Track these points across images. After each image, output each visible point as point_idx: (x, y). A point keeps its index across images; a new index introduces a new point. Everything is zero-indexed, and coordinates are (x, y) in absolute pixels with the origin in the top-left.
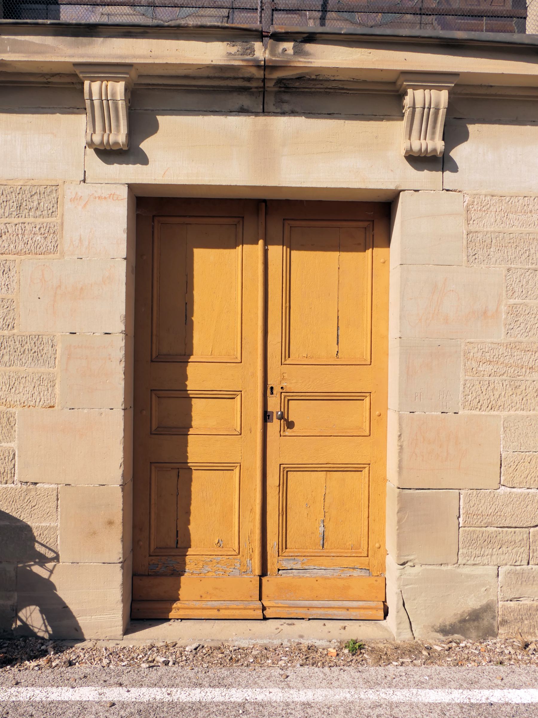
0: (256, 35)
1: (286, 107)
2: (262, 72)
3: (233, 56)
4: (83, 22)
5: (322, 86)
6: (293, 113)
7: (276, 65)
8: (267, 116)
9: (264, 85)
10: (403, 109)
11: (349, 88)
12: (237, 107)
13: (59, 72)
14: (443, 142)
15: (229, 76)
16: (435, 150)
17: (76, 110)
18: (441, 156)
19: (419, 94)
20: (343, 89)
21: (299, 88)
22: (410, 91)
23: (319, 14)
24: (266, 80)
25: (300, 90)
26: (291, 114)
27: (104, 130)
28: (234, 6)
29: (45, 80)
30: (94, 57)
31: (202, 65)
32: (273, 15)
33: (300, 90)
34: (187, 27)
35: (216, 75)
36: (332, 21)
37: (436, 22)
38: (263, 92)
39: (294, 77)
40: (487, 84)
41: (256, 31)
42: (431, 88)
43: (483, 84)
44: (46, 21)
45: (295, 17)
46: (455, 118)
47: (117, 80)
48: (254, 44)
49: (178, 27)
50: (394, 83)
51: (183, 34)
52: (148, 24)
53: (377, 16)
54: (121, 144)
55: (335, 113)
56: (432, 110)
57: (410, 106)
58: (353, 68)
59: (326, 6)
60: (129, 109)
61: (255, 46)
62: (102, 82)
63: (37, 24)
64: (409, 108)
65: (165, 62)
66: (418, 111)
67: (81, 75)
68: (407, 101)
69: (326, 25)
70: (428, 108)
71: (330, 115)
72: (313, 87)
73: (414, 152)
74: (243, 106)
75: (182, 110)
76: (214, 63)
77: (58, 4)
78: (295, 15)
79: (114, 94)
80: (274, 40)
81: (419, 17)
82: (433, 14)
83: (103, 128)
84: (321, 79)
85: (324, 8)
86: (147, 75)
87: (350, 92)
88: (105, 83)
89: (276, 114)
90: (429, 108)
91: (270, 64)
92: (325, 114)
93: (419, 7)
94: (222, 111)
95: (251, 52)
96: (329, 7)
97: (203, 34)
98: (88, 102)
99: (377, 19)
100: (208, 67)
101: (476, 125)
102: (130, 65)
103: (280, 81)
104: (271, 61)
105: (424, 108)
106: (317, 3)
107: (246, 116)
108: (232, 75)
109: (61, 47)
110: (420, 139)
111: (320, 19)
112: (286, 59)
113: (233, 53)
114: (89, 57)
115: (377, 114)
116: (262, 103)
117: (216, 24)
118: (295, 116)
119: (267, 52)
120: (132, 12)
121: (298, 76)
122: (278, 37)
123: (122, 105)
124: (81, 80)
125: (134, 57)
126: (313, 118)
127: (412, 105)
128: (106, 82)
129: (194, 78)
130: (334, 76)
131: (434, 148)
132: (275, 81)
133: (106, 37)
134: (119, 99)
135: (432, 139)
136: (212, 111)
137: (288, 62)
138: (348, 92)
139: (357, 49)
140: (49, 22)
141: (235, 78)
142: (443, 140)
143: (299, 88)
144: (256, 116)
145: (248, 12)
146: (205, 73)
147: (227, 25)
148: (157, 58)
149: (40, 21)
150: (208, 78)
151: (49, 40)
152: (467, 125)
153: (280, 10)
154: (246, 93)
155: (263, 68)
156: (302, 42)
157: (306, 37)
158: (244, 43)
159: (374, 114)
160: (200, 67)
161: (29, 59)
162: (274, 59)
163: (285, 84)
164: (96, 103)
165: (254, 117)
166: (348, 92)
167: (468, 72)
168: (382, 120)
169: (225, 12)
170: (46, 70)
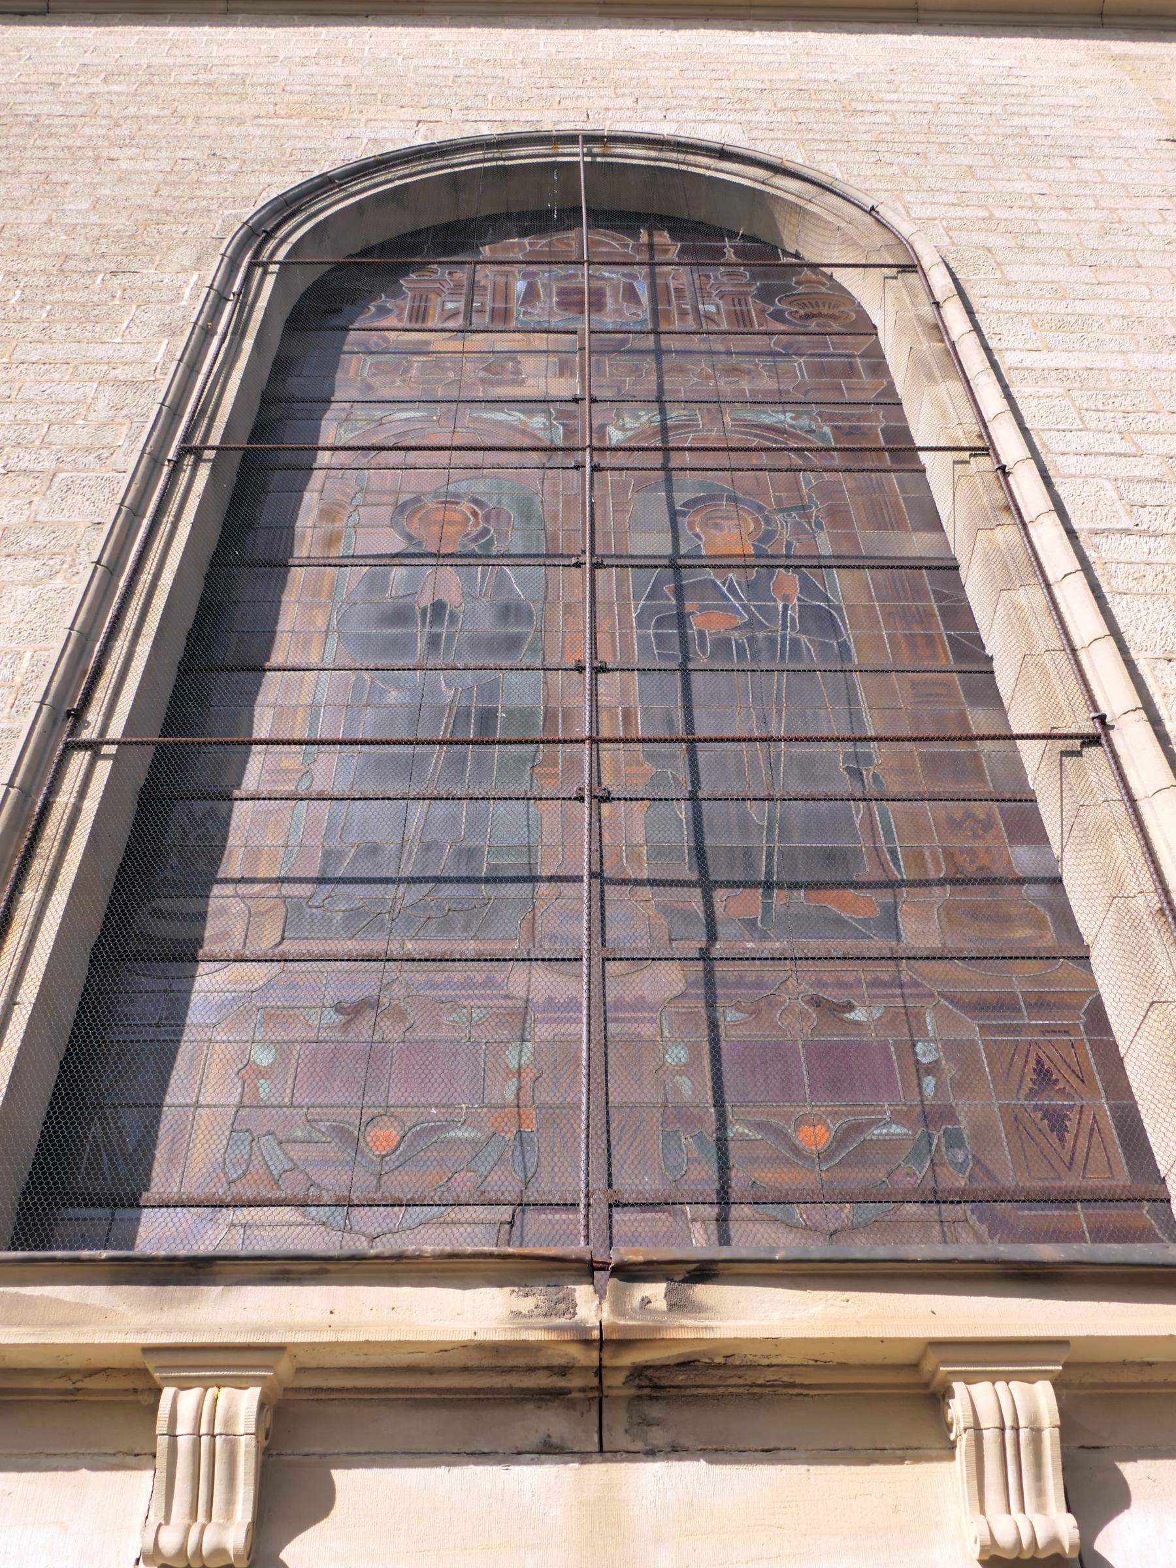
0: (578, 1269)
1: (658, 1436)
2: (595, 1354)
3: (524, 1320)
4: (182, 1253)
5: (741, 1382)
6: (676, 1451)
7: (627, 1337)
8: (611, 1461)
9: (600, 1381)
10: (951, 1431)
11: (806, 1382)
12: (534, 1439)
13: (104, 1365)
14: (1071, 1517)
15: (515, 1363)
16: (1055, 1541)
17: (131, 1460)
18: (1076, 1555)
19: (982, 1391)
20: (793, 1385)
21: (686, 1387)
22: (958, 1387)
23: (713, 1211)
24: (603, 1372)
25: (689, 1392)
26: (671, 1455)
27: (193, 1514)
28: (525, 1200)
29: (69, 1385)
30: (195, 1331)
31: (452, 1342)
32: (610, 1217)
33: (689, 1392)
34: (419, 1257)
35: (485, 1363)
36: (744, 1225)
37: (974, 1217)
38: (599, 1399)
39: (672, 1363)
40: (1139, 1360)
41: (579, 1260)
42: (1008, 1377)
43: (1130, 1359)
44: (98, 1252)
45: (661, 1219)
46: (1083, 1447)
47: (241, 1383)
48: (574, 1290)
49: (400, 1257)
50: (915, 1366)
51: (409, 1271)
52: (331, 1254)
53: (842, 1210)
54: (232, 1553)
55: (782, 1446)
56: (1024, 1434)
57: (968, 1425)
58: (812, 1339)
59: (726, 1193)
60: (264, 1454)
61: (577, 1294)
62: (206, 1390)
63: (77, 1260)
64: (965, 1430)
65: (361, 1339)
66: (990, 1438)
67: (157, 1375)
68: (957, 1410)
69: (733, 1243)
70: (1013, 1428)
71: (770, 1453)
72: (721, 1383)
73: (1003, 1549)
74: (549, 1436)
75: (396, 1453)
76: (481, 1337)
77: (138, 1206)
78: (660, 1214)
79: (229, 1420)
80: (621, 1280)
81: (935, 1207)
82: (966, 1202)
83: (191, 1508)
84: (738, 1363)
85: (722, 1198)
86: (317, 1368)
87: (812, 1392)
88: (212, 1391)
89: (632, 1455)
90: (1016, 1429)
91: (615, 1337)
92: (756, 1451)
93: (929, 1187)
94: (496, 1453)
95: (568, 1309)
96: (734, 1195)
97: (454, 1271)
98: (162, 1443)
99: (843, 1216)
100: (465, 1346)
101: (1140, 1462)
102: (280, 1348)
103: (638, 1372)
104: (615, 1328)
105: (1002, 1429)
106: (706, 1187)
107: (557, 1463)
108: (522, 1361)
109: (121, 1309)
110: (1009, 1512)
111: (717, 1220)
112: (651, 1323)
113: (525, 1312)
114: (182, 1331)
115: (887, 1446)
116: (596, 1428)
117: (486, 1249)
118: (680, 1459)
119: (606, 1306)
120: (300, 1219)
121: (681, 1360)
122: (629, 1273)
123: (247, 1446)
124: (155, 1382)
125: (291, 1328)
126: (726, 1463)
127: (971, 1423)
128: (215, 1389)
129: (430, 1371)
130: (768, 1357)
131: (1051, 1534)
132: (627, 1373)
133: (231, 1285)
134: (242, 1432)
135: (1041, 1507)
136: (473, 1454)
137: (657, 1329)
138: (805, 1392)
139: (816, 1292)
140: (104, 1254)
141: (531, 1369)
142: (1069, 1510)
143: (686, 1387)
144: (582, 1463)
145: (556, 1212)
146: (459, 1360)
147: (511, 1250)
148: (343, 1329)
149: (85, 1253)
150: (465, 1369)
151: (97, 1295)
152: (1117, 1464)
153: (625, 1205)
154: (556, 1404)
155: (598, 1344)
156: (685, 1281)
157: (695, 1270)
158: (550, 1289)
159: (879, 1446)
160: (445, 1348)
161: (40, 1341)
162: (622, 1322)
163: (650, 1380)
164: (184, 1444)
165: (577, 1465)
166: (805, 1392)
167: (1088, 1337)
168: (901, 1460)
169: (505, 1213)
170: (74, 1363)
